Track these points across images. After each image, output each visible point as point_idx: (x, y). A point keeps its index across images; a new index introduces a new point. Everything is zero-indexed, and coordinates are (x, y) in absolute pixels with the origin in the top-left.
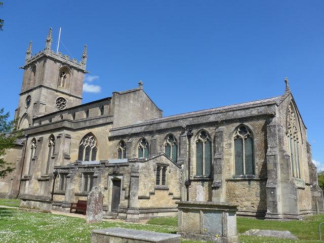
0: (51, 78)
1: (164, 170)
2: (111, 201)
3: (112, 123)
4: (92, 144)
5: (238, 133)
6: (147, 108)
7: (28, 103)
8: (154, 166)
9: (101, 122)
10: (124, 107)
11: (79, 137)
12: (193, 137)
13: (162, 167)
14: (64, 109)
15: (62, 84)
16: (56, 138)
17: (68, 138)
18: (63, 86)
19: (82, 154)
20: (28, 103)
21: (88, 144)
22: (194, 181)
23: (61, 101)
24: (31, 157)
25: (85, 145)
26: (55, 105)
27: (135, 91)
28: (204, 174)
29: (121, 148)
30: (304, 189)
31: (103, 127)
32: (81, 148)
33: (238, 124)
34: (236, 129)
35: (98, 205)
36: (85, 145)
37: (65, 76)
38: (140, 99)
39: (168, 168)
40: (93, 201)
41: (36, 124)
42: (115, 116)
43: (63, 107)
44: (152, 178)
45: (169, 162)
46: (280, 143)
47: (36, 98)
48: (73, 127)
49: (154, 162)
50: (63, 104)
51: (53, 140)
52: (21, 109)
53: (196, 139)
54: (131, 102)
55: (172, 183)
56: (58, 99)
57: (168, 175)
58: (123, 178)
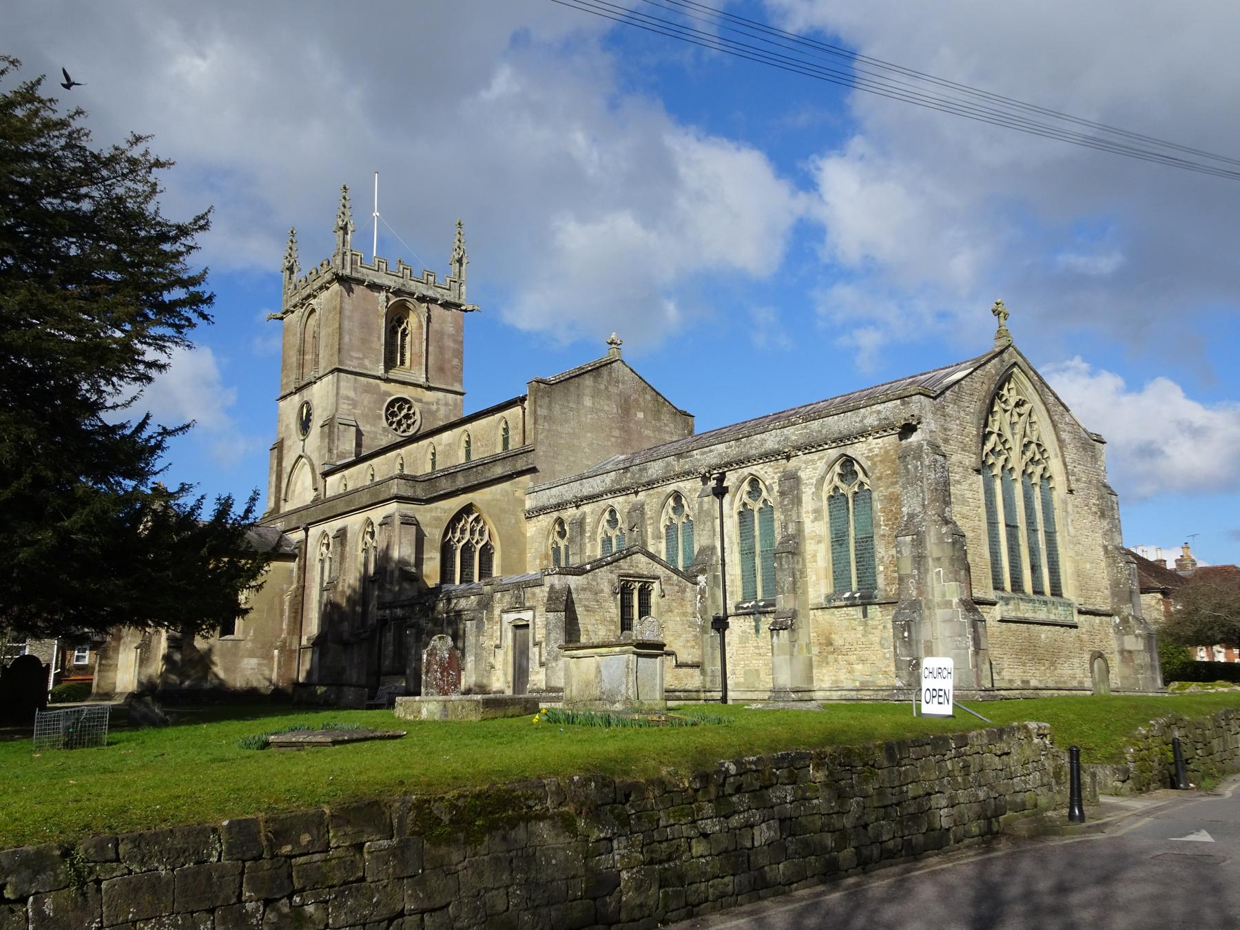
0: (364, 341)
1: (645, 593)
2: (510, 679)
5: (836, 479)
6: (640, 415)
7: (305, 425)
8: (611, 582)
9: (499, 471)
10: (567, 421)
11: (438, 519)
13: (638, 585)
14: (412, 431)
16: (377, 529)
20: (305, 425)
21: (467, 536)
23: (400, 409)
24: (321, 584)
25: (477, 543)
27: (596, 370)
28: (759, 597)
29: (558, 539)
31: (506, 486)
33: (833, 453)
34: (831, 466)
35: (449, 674)
38: (613, 390)
39: (656, 586)
41: (334, 484)
43: (409, 426)
44: (607, 615)
45: (659, 570)
46: (581, 549)
47: (325, 409)
48: (420, 494)
49: (611, 572)
50: (407, 417)
52: (287, 443)
53: (737, 506)
54: (588, 402)
56: (392, 404)
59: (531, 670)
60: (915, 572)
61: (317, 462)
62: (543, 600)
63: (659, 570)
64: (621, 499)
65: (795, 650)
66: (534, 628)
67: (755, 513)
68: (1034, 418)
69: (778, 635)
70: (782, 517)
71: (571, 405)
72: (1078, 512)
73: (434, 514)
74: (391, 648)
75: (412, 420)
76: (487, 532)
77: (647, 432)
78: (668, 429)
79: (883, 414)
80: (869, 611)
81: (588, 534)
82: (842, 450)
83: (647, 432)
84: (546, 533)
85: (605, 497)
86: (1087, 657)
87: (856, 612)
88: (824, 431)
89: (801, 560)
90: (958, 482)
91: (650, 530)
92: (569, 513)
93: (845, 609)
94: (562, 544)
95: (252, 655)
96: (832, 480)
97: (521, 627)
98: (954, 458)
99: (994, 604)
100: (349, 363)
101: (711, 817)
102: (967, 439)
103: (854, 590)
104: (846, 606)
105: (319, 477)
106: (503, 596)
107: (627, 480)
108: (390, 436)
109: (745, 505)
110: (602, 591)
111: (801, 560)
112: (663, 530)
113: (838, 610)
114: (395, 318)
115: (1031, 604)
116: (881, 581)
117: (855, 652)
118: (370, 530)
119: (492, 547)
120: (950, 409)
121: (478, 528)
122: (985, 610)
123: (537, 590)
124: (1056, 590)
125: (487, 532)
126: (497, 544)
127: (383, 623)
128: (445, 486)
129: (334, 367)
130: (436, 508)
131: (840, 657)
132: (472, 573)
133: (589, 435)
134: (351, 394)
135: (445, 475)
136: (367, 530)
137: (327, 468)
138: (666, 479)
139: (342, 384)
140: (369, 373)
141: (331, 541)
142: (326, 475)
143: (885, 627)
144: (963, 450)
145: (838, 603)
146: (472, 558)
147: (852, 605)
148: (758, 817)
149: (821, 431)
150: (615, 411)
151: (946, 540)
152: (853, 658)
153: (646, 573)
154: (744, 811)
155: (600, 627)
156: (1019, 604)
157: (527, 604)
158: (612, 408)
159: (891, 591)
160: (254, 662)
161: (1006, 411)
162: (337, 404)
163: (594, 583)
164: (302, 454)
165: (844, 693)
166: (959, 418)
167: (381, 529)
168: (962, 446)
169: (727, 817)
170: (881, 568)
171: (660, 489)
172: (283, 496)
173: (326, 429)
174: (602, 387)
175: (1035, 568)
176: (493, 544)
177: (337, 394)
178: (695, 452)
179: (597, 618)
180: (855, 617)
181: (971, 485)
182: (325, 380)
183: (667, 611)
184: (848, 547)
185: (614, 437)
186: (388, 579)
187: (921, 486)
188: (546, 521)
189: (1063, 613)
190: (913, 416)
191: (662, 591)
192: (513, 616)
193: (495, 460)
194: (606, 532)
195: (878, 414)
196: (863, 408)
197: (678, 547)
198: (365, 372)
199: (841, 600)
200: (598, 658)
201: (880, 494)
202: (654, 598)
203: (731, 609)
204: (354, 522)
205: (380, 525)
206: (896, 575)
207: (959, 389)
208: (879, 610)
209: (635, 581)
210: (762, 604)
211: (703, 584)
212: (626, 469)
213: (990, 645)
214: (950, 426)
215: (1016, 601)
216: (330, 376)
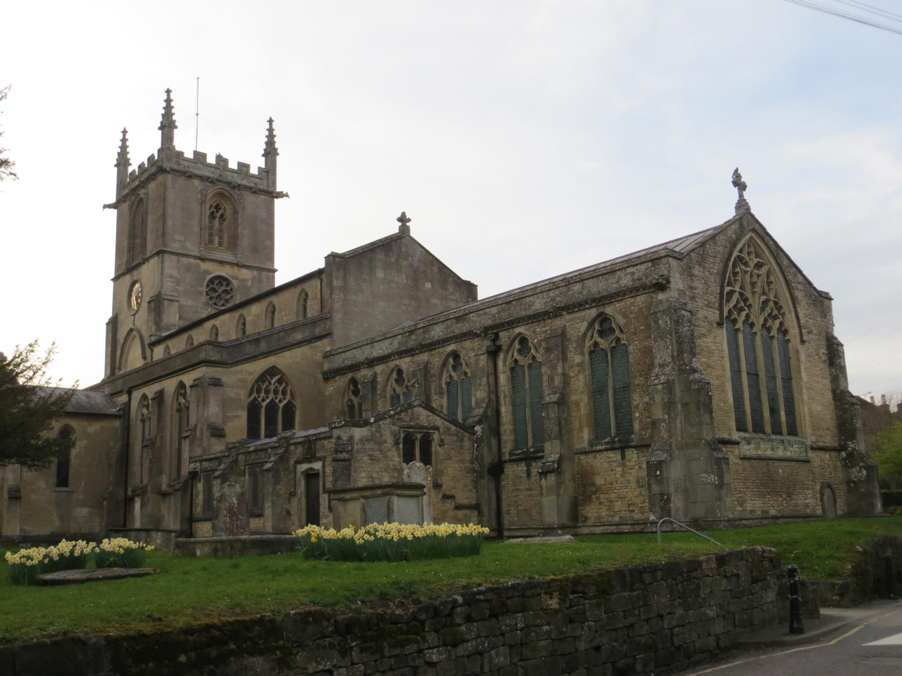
3: (328, 335)
4: (280, 396)
5: (596, 335)
6: (428, 285)
8: (393, 434)
12: (501, 356)
13: (419, 436)
15: (216, 239)
17: (215, 385)
18: (220, 244)
19: (258, 423)
21: (271, 396)
22: (510, 461)
23: (220, 284)
26: (204, 298)
28: (530, 443)
29: (353, 397)
30: (807, 461)
32: (253, 410)
33: (593, 312)
34: (591, 324)
35: (238, 519)
36: (263, 400)
37: (222, 216)
40: (225, 512)
41: (159, 353)
42: (337, 317)
43: (227, 301)
44: (391, 463)
45: (439, 422)
48: (225, 357)
49: (394, 424)
51: (356, 392)
53: (509, 361)
54: (380, 274)
55: (450, 471)
56: (212, 281)
57: (437, 452)
58: (324, 466)
59: (321, 514)
60: (666, 417)
61: (145, 335)
62: (331, 451)
63: (439, 422)
64: (407, 360)
65: (562, 491)
66: (324, 476)
67: (526, 368)
68: (772, 279)
69: (546, 478)
70: (549, 372)
71: (364, 276)
72: (810, 361)
73: (239, 376)
74: (201, 497)
75: (230, 296)
76: (289, 392)
77: (434, 301)
78: (453, 297)
79: (636, 275)
80: (626, 453)
81: (379, 392)
82: (601, 309)
83: (434, 301)
84: (342, 392)
85: (393, 358)
86: (818, 487)
87: (615, 456)
88: (585, 292)
89: (566, 409)
90: (704, 335)
91: (433, 386)
92: (362, 374)
93: (606, 453)
94: (355, 400)
95: (84, 504)
96: (592, 337)
97: (311, 476)
98: (701, 314)
99: (737, 443)
100: (173, 245)
101: (438, 647)
102: (712, 297)
103: (613, 435)
104: (607, 450)
105: (147, 346)
106: (296, 448)
107: (411, 344)
108: (210, 309)
109: (516, 361)
110: (385, 442)
111: (566, 409)
112: (444, 386)
113: (600, 453)
114: (214, 205)
115: (770, 443)
116: (636, 426)
117: (615, 491)
118: (183, 392)
119: (294, 406)
120: (697, 271)
121: (281, 389)
122: (729, 449)
123: (326, 442)
124: (793, 430)
125: (289, 392)
126: (298, 404)
127: (194, 475)
128: (250, 349)
129: (159, 249)
130: (242, 370)
131: (601, 495)
132: (265, 430)
133: (381, 303)
134: (175, 273)
135: (249, 341)
136: (181, 391)
137: (153, 339)
138: (445, 341)
139: (166, 264)
140: (191, 253)
141: (150, 402)
142: (153, 345)
143: (640, 468)
144: (708, 306)
145: (599, 448)
146: (276, 416)
147: (612, 449)
148: (486, 644)
149: (581, 292)
150: (405, 281)
151: (693, 387)
152: (613, 496)
153: (426, 424)
154: (473, 639)
155: (384, 474)
156: (759, 443)
157: (318, 455)
158: (402, 279)
159: (646, 434)
160: (85, 511)
161: (746, 272)
162: (162, 281)
163: (378, 434)
164: (133, 327)
165: (606, 528)
166: (703, 278)
167: (191, 390)
168: (706, 303)
169: (455, 645)
170: (637, 415)
171: (441, 350)
172: (117, 364)
173: (153, 305)
174: (393, 260)
175: (774, 411)
176: (294, 403)
177: (162, 273)
178: (471, 315)
179: (381, 466)
180: (614, 459)
181: (715, 337)
182: (152, 261)
183: (446, 459)
184: (608, 396)
185: (405, 305)
186: (198, 435)
187: (670, 339)
188: (341, 382)
189: (798, 450)
190: (662, 276)
191: (442, 440)
192: (304, 467)
193: (294, 328)
194: (394, 390)
195: (632, 275)
196: (619, 270)
197: (458, 401)
198: (187, 253)
199: (602, 445)
200: (362, 500)
201: (635, 348)
202: (435, 447)
203: (506, 457)
204: (170, 385)
205: (191, 387)
206: (649, 420)
207: (704, 252)
208: (635, 452)
209: (416, 432)
210: (532, 450)
211: (479, 433)
212: (411, 332)
213: (732, 480)
214: (696, 284)
215: (757, 441)
216: (156, 258)
